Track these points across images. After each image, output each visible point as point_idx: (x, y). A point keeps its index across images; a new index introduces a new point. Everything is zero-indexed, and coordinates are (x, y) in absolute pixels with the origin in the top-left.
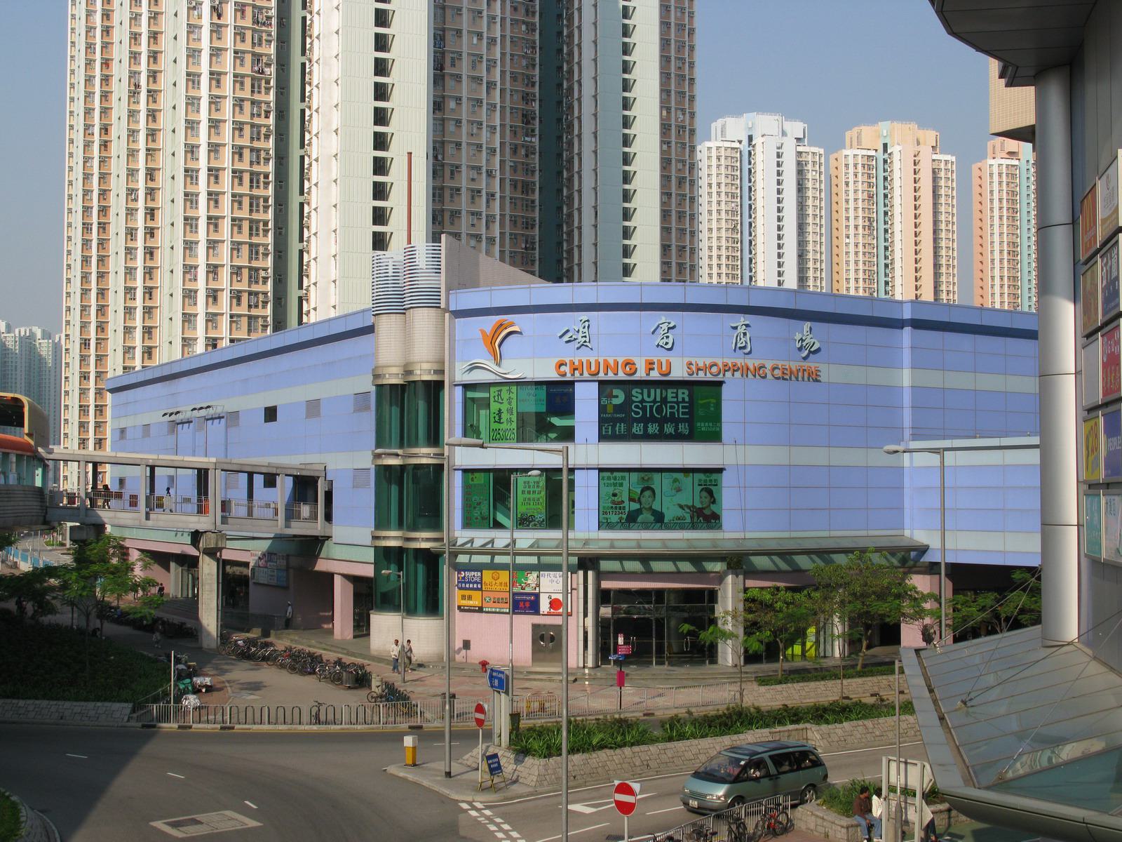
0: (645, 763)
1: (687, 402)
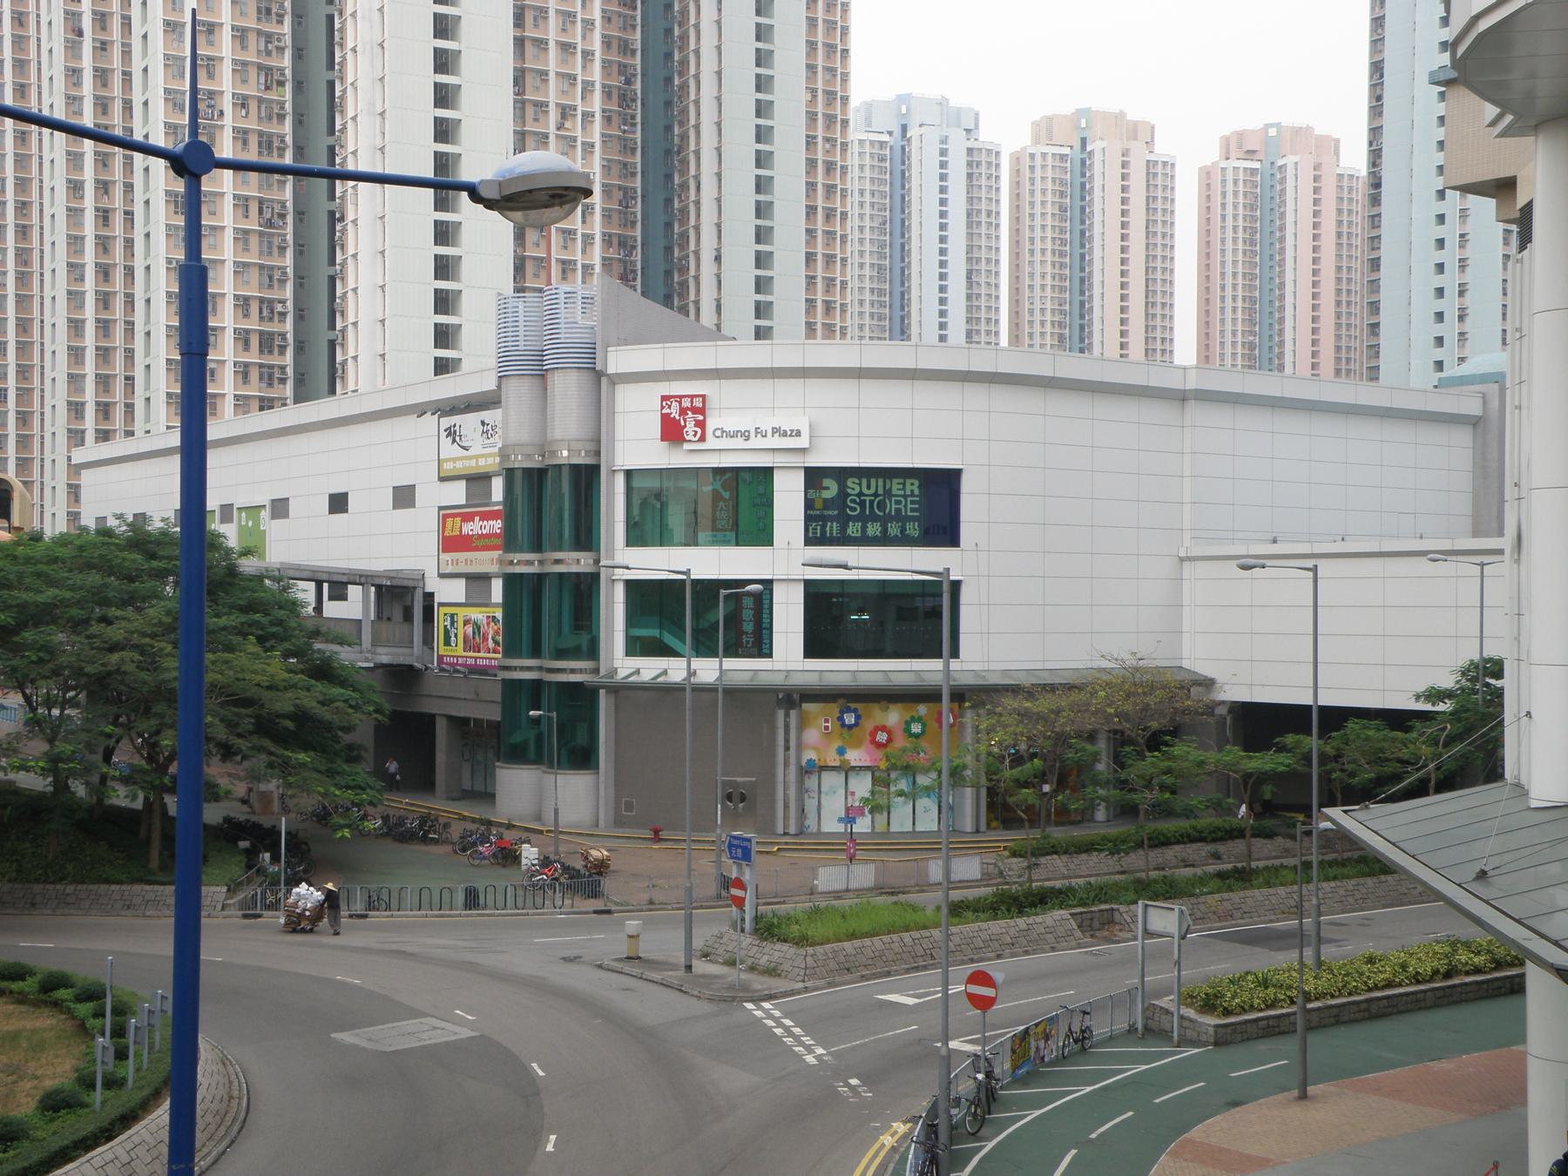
0: (928, 952)
1: (917, 496)
